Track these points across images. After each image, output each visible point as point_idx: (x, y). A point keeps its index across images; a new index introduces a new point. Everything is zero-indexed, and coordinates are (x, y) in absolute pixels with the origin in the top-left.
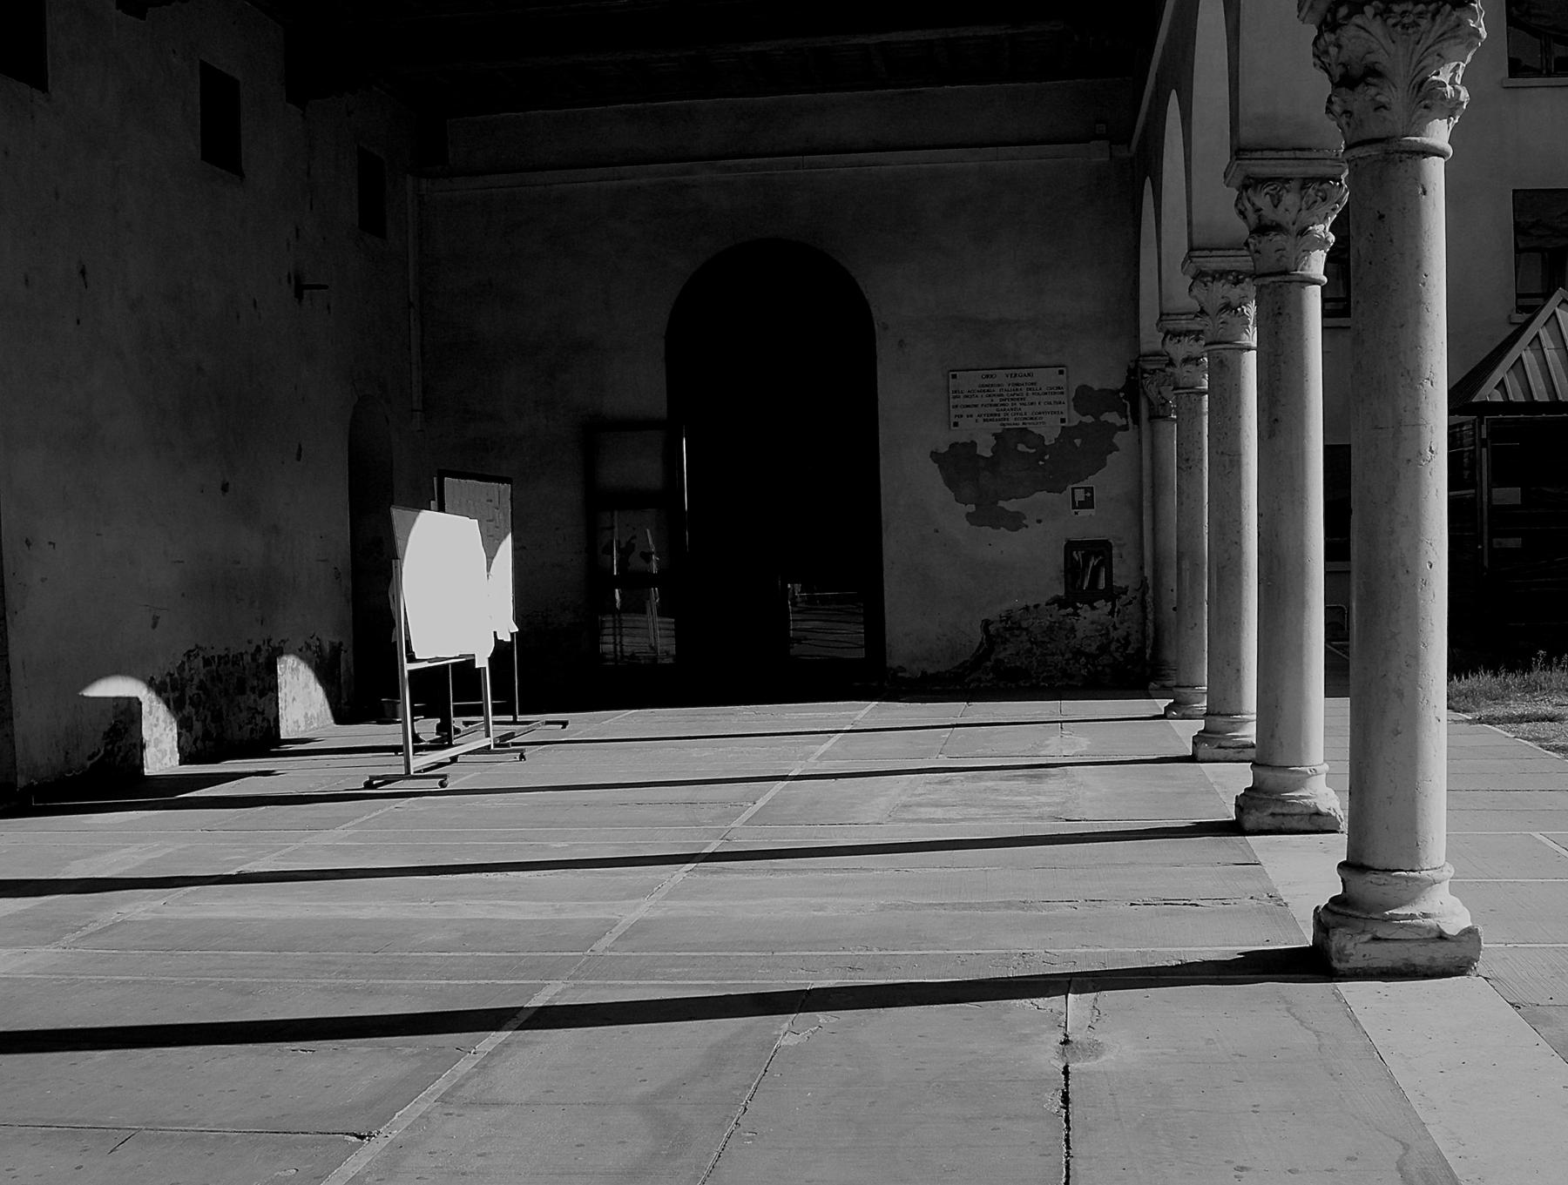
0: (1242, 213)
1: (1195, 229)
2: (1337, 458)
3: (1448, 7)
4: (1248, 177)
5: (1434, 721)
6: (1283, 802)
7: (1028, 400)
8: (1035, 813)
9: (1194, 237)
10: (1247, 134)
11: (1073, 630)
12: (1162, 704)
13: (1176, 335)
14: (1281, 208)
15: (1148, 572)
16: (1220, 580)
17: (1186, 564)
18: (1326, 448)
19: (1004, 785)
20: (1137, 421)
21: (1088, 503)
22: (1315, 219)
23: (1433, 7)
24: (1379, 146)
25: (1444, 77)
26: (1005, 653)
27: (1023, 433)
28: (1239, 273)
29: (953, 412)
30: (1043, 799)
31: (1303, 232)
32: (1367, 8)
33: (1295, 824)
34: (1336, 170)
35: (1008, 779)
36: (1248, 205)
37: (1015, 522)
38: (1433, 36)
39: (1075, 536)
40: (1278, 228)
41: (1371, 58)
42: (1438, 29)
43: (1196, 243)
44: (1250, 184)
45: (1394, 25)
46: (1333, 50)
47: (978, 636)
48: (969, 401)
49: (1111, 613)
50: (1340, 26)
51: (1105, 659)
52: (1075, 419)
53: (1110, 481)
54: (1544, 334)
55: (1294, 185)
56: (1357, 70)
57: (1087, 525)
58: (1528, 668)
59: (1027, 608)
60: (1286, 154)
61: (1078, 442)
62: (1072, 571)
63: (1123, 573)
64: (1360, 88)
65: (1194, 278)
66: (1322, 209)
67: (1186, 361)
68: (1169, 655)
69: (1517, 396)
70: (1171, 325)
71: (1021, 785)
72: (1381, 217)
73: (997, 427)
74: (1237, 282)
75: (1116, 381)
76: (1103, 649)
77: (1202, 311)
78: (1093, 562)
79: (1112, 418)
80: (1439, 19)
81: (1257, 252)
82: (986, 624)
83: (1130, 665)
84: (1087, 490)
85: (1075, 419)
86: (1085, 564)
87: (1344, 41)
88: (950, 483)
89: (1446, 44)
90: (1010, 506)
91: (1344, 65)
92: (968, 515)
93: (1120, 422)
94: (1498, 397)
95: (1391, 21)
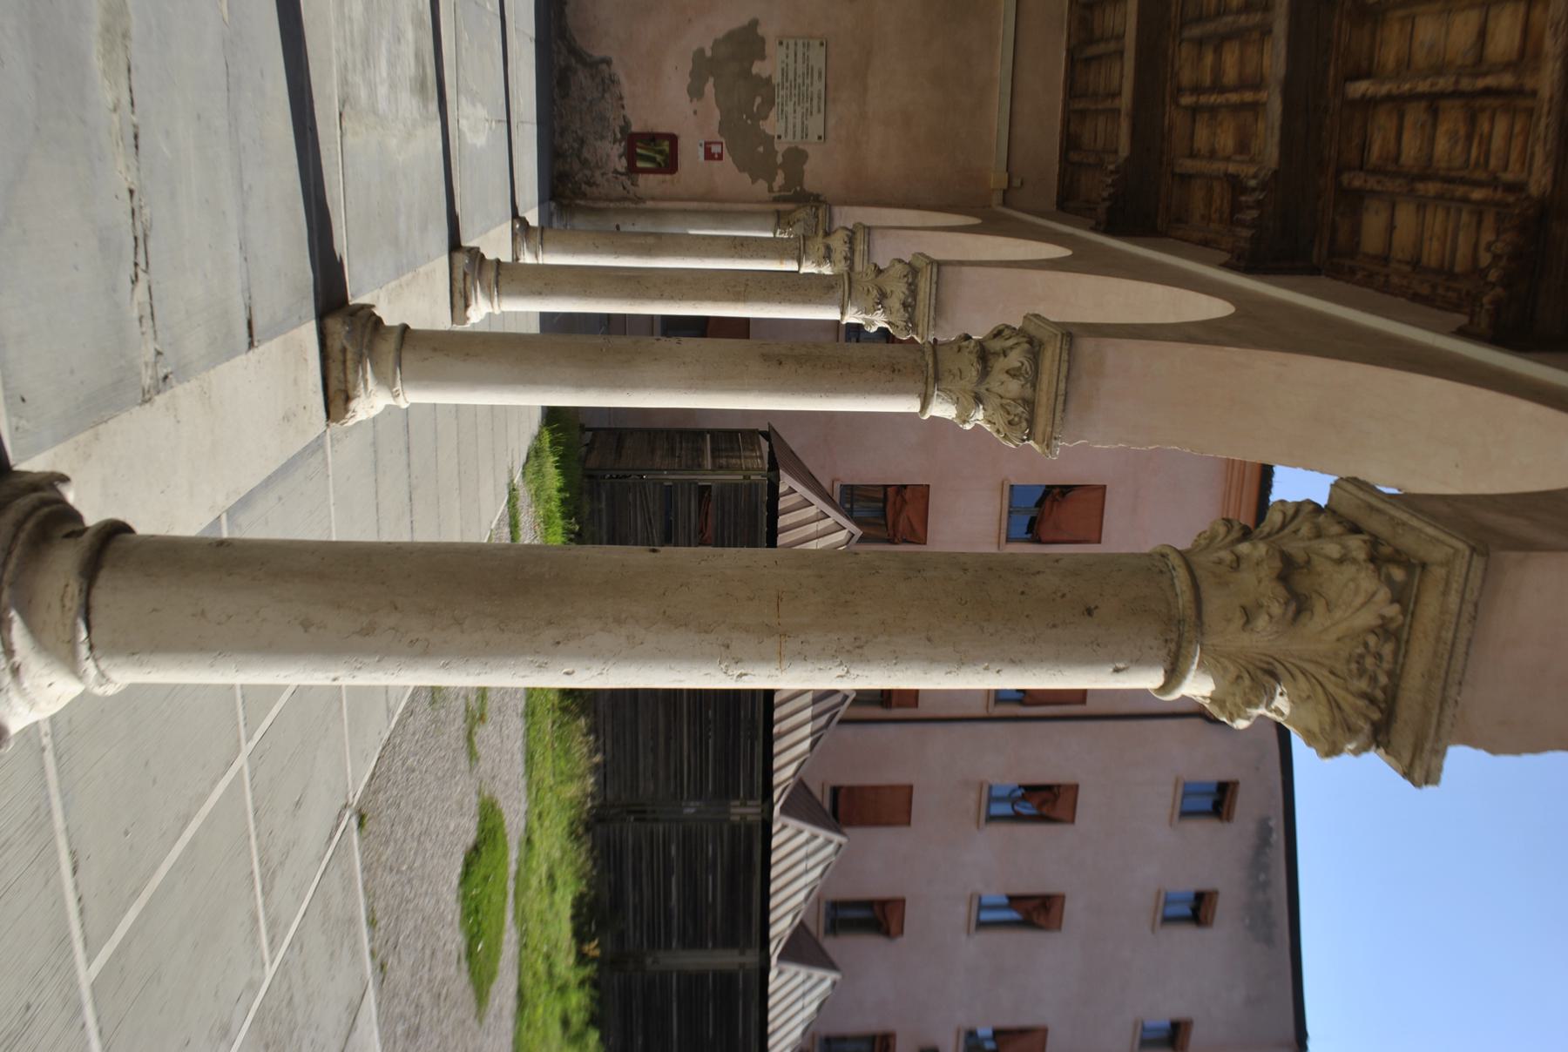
0: (997, 334)
1: (957, 269)
2: (741, 328)
3: (1376, 716)
4: (1041, 344)
5: (332, 675)
6: (359, 361)
7: (798, 109)
8: (356, 79)
9: (966, 269)
10: (1087, 345)
11: (602, 138)
12: (533, 219)
13: (851, 241)
14: (1005, 377)
15: (650, 204)
16: (629, 278)
17: (651, 240)
18: (747, 320)
19: (408, 50)
20: (776, 200)
21: (709, 155)
22: (990, 412)
23: (1379, 694)
24: (1191, 613)
25: (1282, 703)
26: (582, 77)
27: (770, 102)
28: (914, 307)
29: (792, 42)
30: (383, 91)
31: (978, 400)
32: (1396, 608)
33: (335, 373)
34: (1039, 436)
35: (418, 56)
36: (1010, 342)
37: (695, 92)
38: (1340, 694)
39: (682, 143)
40: (985, 373)
41: (1319, 607)
42: (1348, 701)
43: (944, 269)
44: (1035, 347)
45: (1366, 645)
46: (1333, 550)
47: (597, 53)
48: (800, 55)
49: (616, 171)
50: (1378, 570)
51: (576, 166)
52: (780, 147)
53: (726, 174)
54: (829, 522)
55: (1028, 392)
56: (1303, 583)
57: (691, 153)
58: (566, 516)
59: (621, 98)
60: (1062, 386)
61: (761, 149)
62: (652, 138)
63: (649, 183)
64: (1280, 591)
65: (909, 264)
66: (1000, 420)
67: (828, 248)
68: (579, 222)
69: (783, 504)
70: (860, 236)
71: (408, 67)
72: (1089, 612)
73: (777, 79)
74: (905, 305)
75: (810, 184)
76: (585, 163)
77: (879, 271)
78: (659, 158)
79: (780, 179)
80: (1361, 703)
81: (960, 350)
82: (608, 62)
83: (572, 190)
84: (720, 157)
85: (780, 147)
86: (656, 151)
87: (1349, 570)
88: (731, 36)
89: (1324, 709)
90: (709, 88)
91: (1309, 562)
92: (701, 51)
93: (776, 188)
94: (782, 489)
95: (1372, 640)
